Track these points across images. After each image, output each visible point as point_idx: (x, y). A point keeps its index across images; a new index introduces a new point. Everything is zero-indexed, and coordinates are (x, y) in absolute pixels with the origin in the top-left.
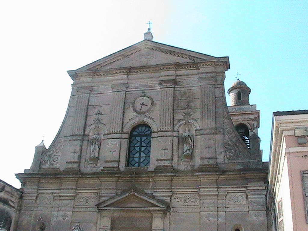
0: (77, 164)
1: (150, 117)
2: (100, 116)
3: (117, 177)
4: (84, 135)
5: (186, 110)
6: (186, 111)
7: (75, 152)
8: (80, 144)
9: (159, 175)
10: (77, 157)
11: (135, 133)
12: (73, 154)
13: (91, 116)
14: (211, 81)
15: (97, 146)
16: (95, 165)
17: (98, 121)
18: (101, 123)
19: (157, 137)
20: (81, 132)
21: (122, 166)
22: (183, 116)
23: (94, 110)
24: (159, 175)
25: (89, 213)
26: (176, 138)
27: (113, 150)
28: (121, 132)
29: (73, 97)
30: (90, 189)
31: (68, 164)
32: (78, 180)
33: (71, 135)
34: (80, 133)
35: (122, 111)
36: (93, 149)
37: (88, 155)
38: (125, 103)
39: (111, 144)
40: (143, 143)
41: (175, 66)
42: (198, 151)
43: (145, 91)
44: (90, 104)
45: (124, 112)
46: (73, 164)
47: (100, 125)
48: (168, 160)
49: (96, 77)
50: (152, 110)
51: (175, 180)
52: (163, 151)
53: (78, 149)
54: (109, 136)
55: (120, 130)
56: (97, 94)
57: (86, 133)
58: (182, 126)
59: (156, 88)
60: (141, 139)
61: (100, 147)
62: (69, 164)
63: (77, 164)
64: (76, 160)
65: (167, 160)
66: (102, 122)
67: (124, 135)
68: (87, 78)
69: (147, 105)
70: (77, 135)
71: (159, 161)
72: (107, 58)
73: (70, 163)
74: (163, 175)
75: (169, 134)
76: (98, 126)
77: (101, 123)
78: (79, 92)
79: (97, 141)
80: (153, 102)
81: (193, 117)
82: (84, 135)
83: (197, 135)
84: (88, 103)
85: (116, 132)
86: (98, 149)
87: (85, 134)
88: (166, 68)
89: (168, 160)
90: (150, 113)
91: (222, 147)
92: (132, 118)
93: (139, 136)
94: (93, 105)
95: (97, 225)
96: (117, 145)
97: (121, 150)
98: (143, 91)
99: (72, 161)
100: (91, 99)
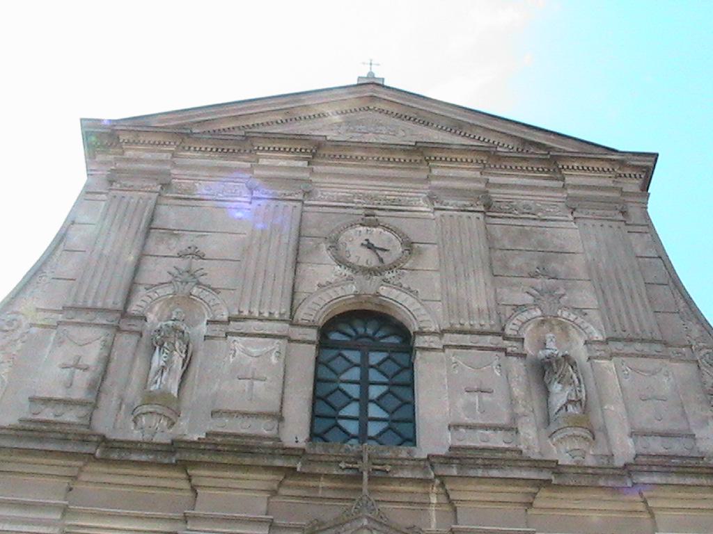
0: (83, 412)
1: (404, 285)
2: (197, 264)
3: (279, 468)
4: (124, 314)
5: (539, 280)
6: (540, 282)
7: (76, 366)
8: (105, 341)
9: (480, 473)
10: (85, 386)
11: (335, 336)
12: (67, 372)
13: (159, 259)
14: (613, 212)
15: (178, 359)
16: (164, 423)
17: (187, 275)
18: (198, 284)
19: (443, 350)
20: (114, 300)
21: (296, 431)
22: (530, 297)
23: (173, 242)
24: (480, 473)
25: (521, 248)
26: (515, 359)
27: (257, 378)
28: (286, 317)
29: (89, 196)
30: (137, 517)
31: (40, 407)
32: (81, 469)
33: (69, 304)
34: (110, 305)
35: (291, 258)
36: (162, 363)
37: (136, 380)
38: (300, 236)
39: (244, 351)
40: (356, 395)
41: (483, 158)
42: (613, 408)
43: (377, 212)
44: (157, 223)
45: (297, 263)
46: (60, 409)
47: (195, 291)
48: (501, 428)
49: (188, 153)
50: (407, 265)
51: (543, 504)
52: (475, 398)
53: (92, 355)
54: (233, 327)
55: (283, 311)
56: (188, 199)
57: (133, 309)
58: (532, 326)
59: (414, 208)
60: (365, 357)
61: (187, 363)
62: (43, 407)
63: (83, 412)
64: (79, 393)
65: (495, 428)
66: (202, 279)
67: (301, 330)
68: (143, 157)
69: (386, 250)
70: (94, 309)
71: (462, 430)
72: (240, 106)
73: (47, 401)
74: (495, 473)
75: (488, 341)
76: (186, 291)
77: (198, 284)
78: (118, 185)
79: (179, 338)
80: (410, 246)
81: (568, 301)
82: (124, 314)
83: (597, 358)
84: (152, 220)
85: (266, 315)
86: (180, 371)
87: (128, 310)
88: (451, 160)
89: (501, 428)
90: (403, 273)
91: (701, 402)
92: (328, 286)
93: (365, 345)
94: (172, 227)
95: (644, 279)
96: (274, 360)
97: (291, 380)
98: (369, 212)
99: (60, 397)
100: (163, 209)
